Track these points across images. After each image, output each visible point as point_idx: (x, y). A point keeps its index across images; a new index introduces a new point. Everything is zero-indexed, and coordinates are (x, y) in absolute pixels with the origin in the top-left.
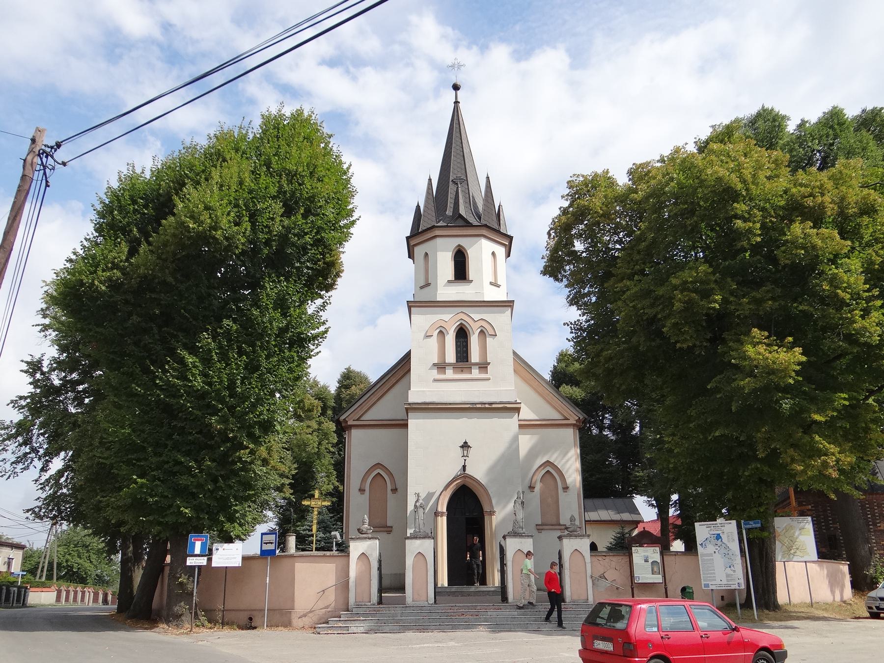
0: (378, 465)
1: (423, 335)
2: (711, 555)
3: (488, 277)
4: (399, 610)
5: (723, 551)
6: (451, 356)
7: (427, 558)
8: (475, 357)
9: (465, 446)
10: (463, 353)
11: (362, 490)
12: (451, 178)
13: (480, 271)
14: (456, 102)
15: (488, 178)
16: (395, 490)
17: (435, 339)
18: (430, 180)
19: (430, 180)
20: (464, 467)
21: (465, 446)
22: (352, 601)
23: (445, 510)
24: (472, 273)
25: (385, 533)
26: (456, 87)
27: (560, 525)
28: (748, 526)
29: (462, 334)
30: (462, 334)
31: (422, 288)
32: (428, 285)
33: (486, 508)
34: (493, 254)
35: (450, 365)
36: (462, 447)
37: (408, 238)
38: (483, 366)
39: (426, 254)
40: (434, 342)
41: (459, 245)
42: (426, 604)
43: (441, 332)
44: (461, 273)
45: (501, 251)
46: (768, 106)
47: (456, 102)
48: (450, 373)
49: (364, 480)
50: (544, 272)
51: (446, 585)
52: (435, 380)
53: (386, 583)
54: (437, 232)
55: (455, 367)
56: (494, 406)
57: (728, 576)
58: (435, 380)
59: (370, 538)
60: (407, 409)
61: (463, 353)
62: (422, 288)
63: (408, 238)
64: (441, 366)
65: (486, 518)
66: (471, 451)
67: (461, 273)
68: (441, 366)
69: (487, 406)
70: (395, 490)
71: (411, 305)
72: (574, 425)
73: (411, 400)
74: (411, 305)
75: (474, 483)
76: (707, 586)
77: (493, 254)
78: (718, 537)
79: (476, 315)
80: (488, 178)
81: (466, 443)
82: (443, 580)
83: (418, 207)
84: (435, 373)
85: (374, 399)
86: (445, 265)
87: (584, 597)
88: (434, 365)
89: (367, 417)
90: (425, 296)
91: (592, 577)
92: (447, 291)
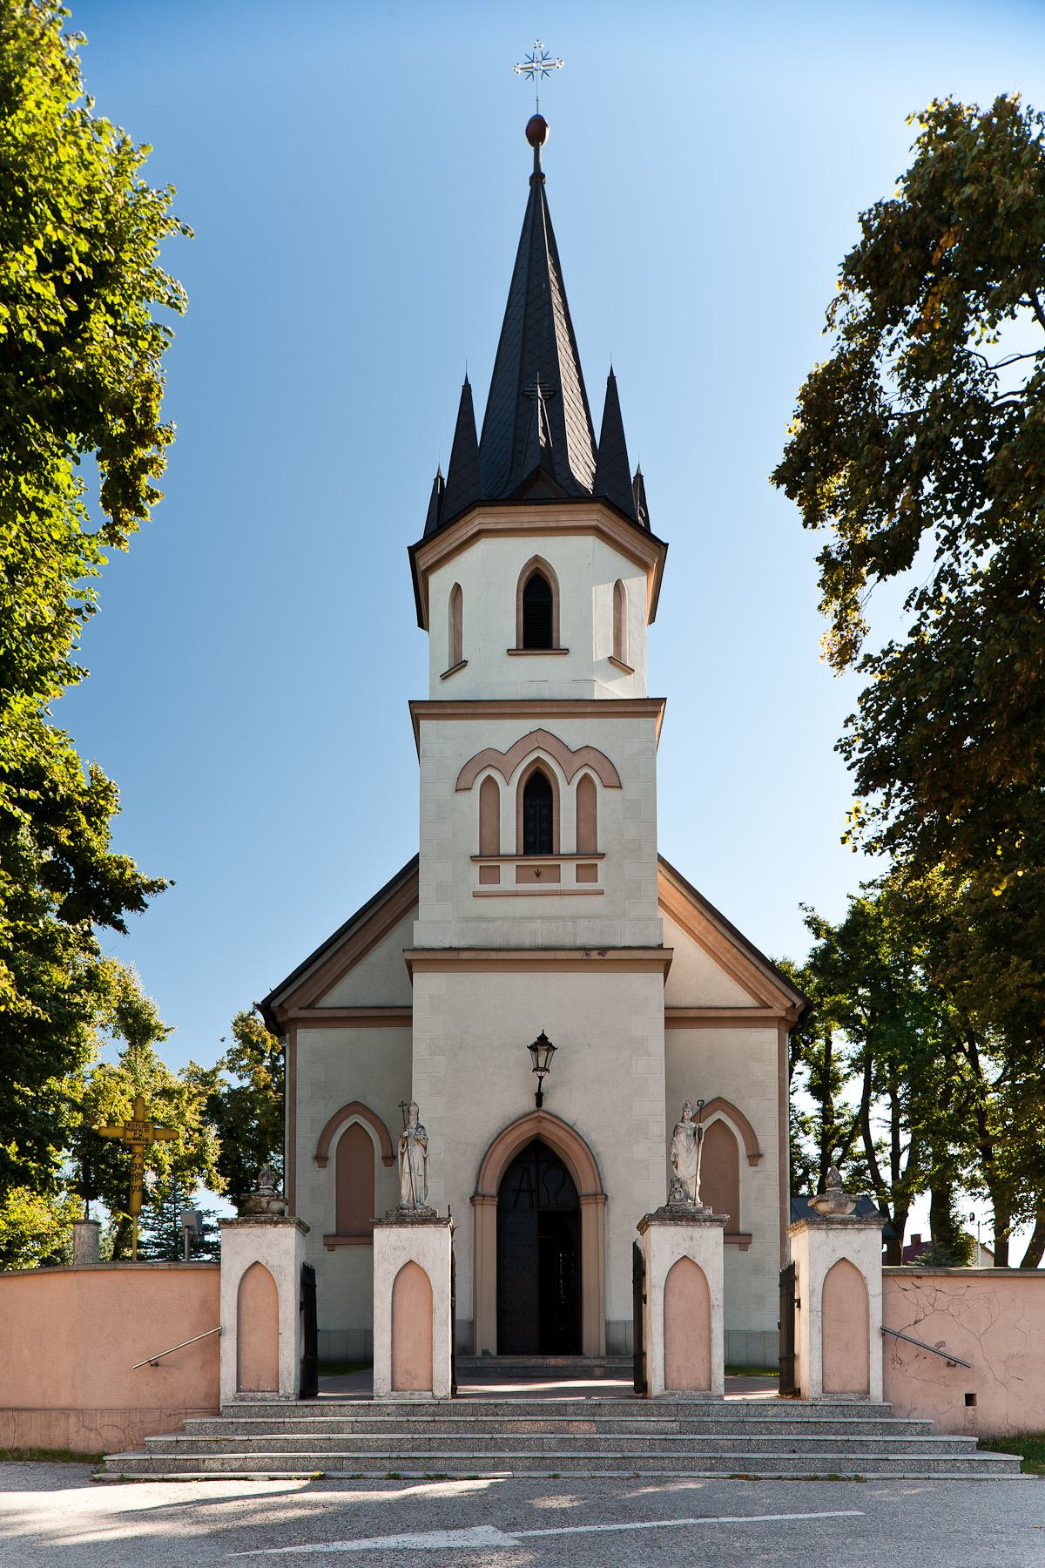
0: (355, 1107)
3: (603, 648)
6: (510, 837)
7: (425, 1275)
8: (567, 839)
10: (538, 834)
11: (321, 1159)
13: (586, 625)
14: (537, 179)
15: (612, 381)
17: (474, 796)
18: (467, 391)
19: (467, 391)
20: (539, 1097)
22: (228, 1388)
24: (565, 631)
27: (738, 1234)
29: (538, 791)
30: (538, 791)
31: (445, 676)
32: (459, 665)
33: (586, 1186)
36: (533, 1048)
38: (588, 857)
39: (457, 589)
40: (471, 801)
41: (536, 559)
42: (425, 1398)
44: (538, 625)
47: (537, 179)
50: (780, 477)
51: (493, 1349)
52: (476, 895)
58: (476, 895)
60: (410, 965)
61: (538, 834)
62: (445, 676)
63: (413, 551)
65: (588, 1212)
67: (538, 625)
71: (420, 711)
72: (782, 1019)
73: (419, 941)
74: (420, 711)
79: (572, 732)
80: (612, 381)
81: (543, 1039)
83: (439, 476)
85: (344, 960)
86: (499, 615)
87: (857, 1385)
90: (456, 689)
91: (884, 1331)
92: (503, 671)
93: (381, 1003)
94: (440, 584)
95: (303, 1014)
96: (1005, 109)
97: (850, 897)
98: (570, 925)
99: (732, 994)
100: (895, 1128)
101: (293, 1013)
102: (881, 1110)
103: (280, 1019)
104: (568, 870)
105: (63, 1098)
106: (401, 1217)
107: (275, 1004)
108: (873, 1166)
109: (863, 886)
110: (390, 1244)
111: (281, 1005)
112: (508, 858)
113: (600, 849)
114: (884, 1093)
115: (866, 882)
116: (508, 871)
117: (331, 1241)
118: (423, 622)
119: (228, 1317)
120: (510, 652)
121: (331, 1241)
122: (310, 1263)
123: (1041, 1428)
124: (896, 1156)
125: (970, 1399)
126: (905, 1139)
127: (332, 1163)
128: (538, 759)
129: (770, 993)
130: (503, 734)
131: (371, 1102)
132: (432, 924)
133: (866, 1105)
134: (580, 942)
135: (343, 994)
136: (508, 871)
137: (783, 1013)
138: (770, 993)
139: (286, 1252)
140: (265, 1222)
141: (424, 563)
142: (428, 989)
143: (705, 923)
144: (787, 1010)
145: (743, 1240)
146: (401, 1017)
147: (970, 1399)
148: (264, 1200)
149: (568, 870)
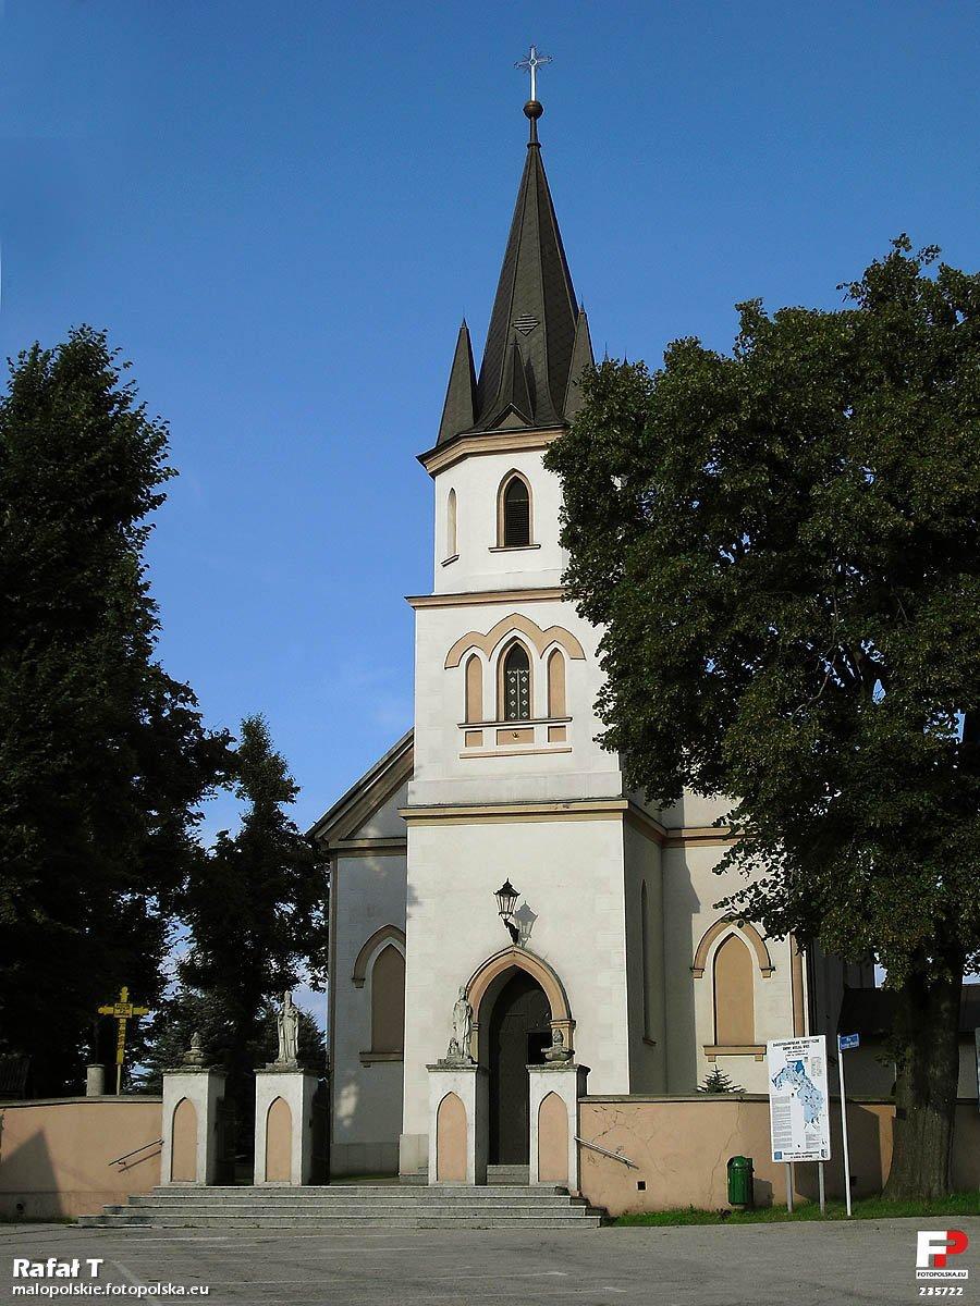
2: (787, 1100)
4: (513, 1192)
5: (805, 1092)
6: (490, 708)
8: (539, 708)
11: (358, 980)
14: (535, 145)
18: (465, 335)
19: (465, 335)
28: (847, 1046)
29: (515, 658)
30: (515, 658)
35: (490, 724)
36: (500, 893)
42: (287, 1184)
46: (172, 457)
47: (535, 145)
49: (361, 960)
54: (464, 448)
57: (809, 1137)
61: (515, 705)
73: (412, 800)
75: (532, 965)
76: (778, 1155)
78: (799, 1067)
95: (342, 845)
96: (244, 820)
104: (541, 731)
112: (490, 724)
116: (489, 734)
117: (367, 1058)
119: (167, 1135)
121: (367, 1058)
125: (642, 1186)
127: (368, 984)
128: (515, 638)
130: (484, 619)
132: (419, 791)
136: (489, 734)
139: (202, 1091)
140: (190, 1072)
142: (419, 837)
145: (758, 1050)
147: (642, 1186)
148: (192, 1057)
149: (541, 731)
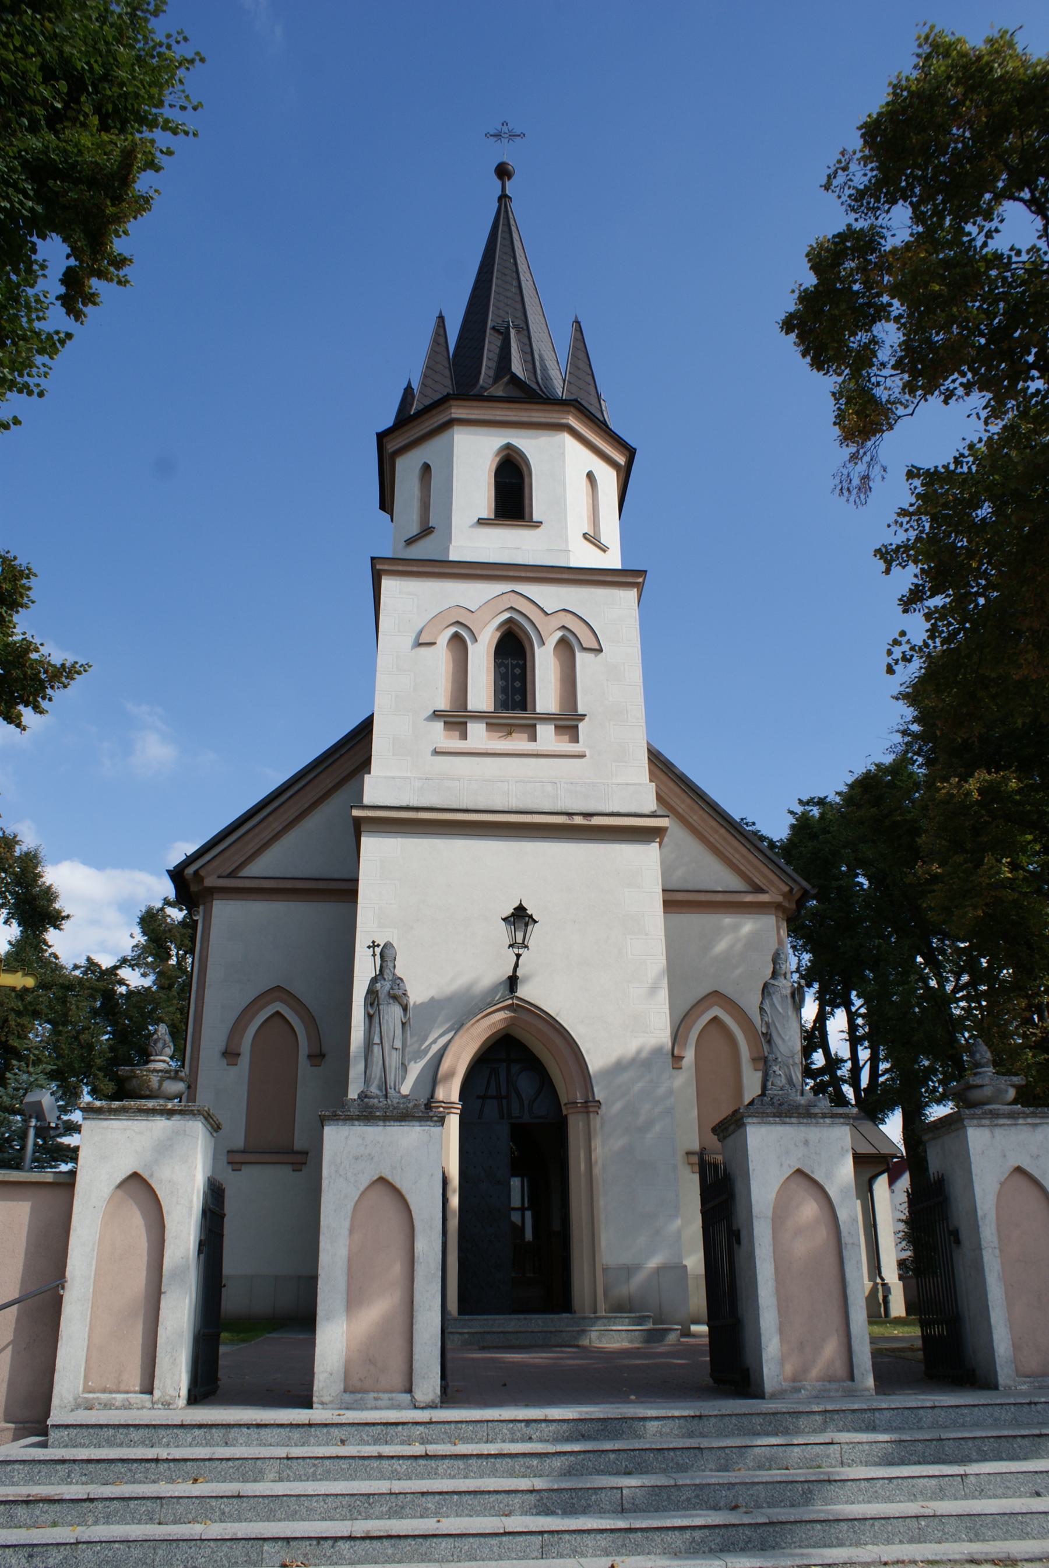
0: (278, 992)
1: (410, 640)
6: (482, 694)
8: (546, 695)
9: (520, 917)
11: (230, 1054)
12: (490, 324)
13: (559, 503)
15: (578, 322)
16: (317, 1057)
18: (441, 318)
19: (441, 318)
21: (520, 917)
23: (455, 1096)
24: (539, 505)
25: (287, 1169)
26: (503, 172)
29: (513, 649)
30: (513, 649)
31: (410, 542)
32: (427, 531)
34: (590, 476)
35: (478, 716)
37: (381, 437)
38: (568, 723)
40: (440, 657)
43: (456, 636)
45: (608, 479)
48: (478, 734)
52: (436, 753)
53: (232, 1301)
55: (493, 725)
56: (596, 821)
59: (170, 1113)
63: (381, 437)
64: (456, 719)
65: (575, 1125)
66: (536, 935)
67: (512, 495)
68: (456, 719)
69: (578, 820)
70: (317, 1057)
77: (590, 476)
79: (550, 597)
82: (458, 1058)
83: (408, 390)
84: (438, 734)
85: (276, 825)
86: (472, 486)
88: (436, 715)
89: (254, 869)
90: (421, 550)
93: (316, 875)
94: (407, 468)
97: (791, 812)
98: (549, 788)
99: (717, 876)
100: (854, 1041)
101: (210, 882)
102: (837, 1024)
103: (194, 888)
105: (40, 1116)
106: (380, 1110)
107: (190, 871)
108: (836, 1082)
109: (801, 802)
110: (347, 1152)
111: (196, 872)
113: (580, 711)
114: (838, 1007)
115: (805, 799)
118: (386, 503)
120: (481, 522)
121: (238, 1158)
122: (219, 1178)
123: (2, 1203)
124: (856, 1070)
126: (864, 1054)
129: (765, 876)
131: (299, 988)
132: (380, 787)
133: (821, 1019)
134: (559, 807)
135: (267, 865)
137: (780, 899)
138: (765, 876)
141: (391, 447)
143: (688, 801)
144: (784, 895)
146: (344, 891)
149: (546, 732)
